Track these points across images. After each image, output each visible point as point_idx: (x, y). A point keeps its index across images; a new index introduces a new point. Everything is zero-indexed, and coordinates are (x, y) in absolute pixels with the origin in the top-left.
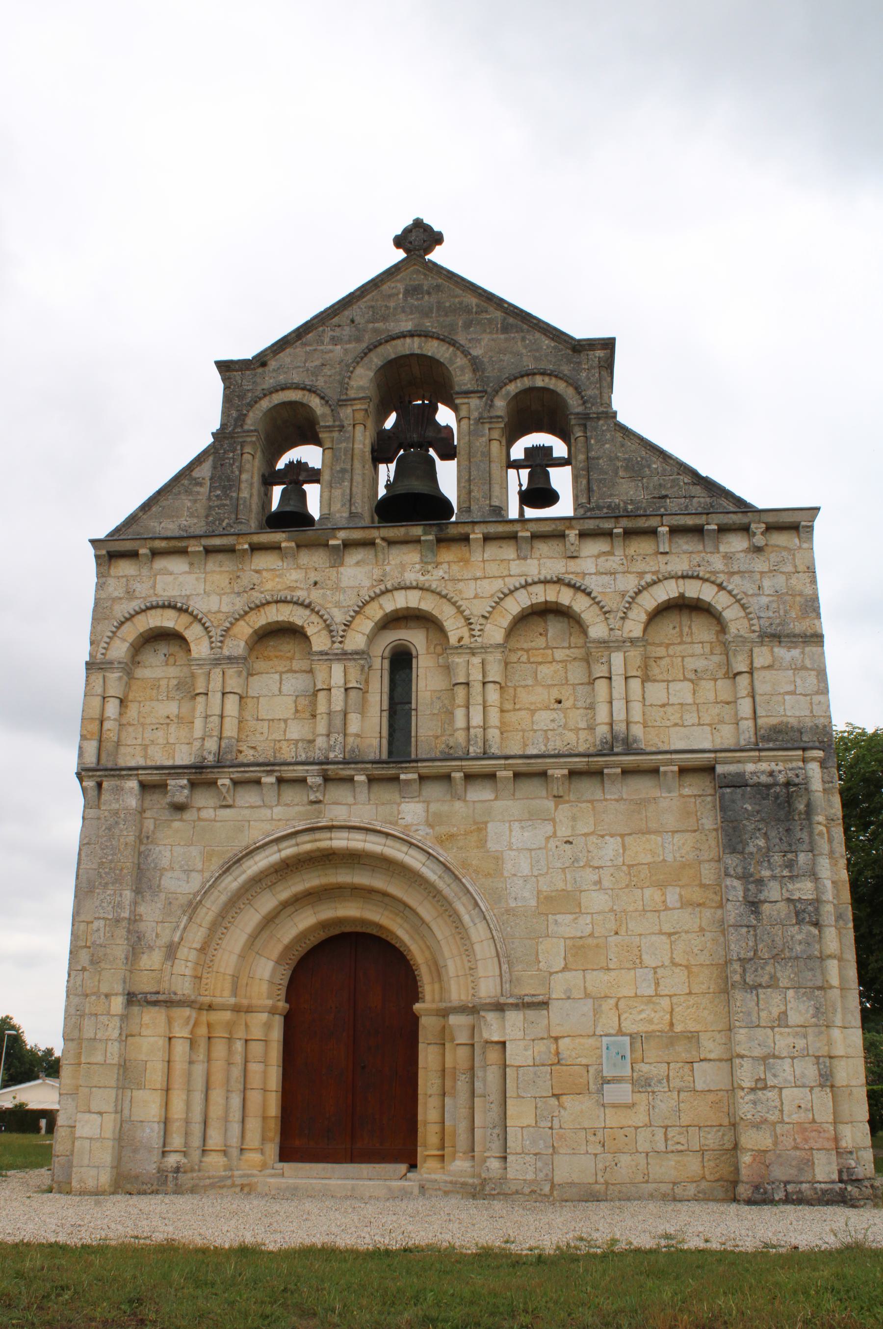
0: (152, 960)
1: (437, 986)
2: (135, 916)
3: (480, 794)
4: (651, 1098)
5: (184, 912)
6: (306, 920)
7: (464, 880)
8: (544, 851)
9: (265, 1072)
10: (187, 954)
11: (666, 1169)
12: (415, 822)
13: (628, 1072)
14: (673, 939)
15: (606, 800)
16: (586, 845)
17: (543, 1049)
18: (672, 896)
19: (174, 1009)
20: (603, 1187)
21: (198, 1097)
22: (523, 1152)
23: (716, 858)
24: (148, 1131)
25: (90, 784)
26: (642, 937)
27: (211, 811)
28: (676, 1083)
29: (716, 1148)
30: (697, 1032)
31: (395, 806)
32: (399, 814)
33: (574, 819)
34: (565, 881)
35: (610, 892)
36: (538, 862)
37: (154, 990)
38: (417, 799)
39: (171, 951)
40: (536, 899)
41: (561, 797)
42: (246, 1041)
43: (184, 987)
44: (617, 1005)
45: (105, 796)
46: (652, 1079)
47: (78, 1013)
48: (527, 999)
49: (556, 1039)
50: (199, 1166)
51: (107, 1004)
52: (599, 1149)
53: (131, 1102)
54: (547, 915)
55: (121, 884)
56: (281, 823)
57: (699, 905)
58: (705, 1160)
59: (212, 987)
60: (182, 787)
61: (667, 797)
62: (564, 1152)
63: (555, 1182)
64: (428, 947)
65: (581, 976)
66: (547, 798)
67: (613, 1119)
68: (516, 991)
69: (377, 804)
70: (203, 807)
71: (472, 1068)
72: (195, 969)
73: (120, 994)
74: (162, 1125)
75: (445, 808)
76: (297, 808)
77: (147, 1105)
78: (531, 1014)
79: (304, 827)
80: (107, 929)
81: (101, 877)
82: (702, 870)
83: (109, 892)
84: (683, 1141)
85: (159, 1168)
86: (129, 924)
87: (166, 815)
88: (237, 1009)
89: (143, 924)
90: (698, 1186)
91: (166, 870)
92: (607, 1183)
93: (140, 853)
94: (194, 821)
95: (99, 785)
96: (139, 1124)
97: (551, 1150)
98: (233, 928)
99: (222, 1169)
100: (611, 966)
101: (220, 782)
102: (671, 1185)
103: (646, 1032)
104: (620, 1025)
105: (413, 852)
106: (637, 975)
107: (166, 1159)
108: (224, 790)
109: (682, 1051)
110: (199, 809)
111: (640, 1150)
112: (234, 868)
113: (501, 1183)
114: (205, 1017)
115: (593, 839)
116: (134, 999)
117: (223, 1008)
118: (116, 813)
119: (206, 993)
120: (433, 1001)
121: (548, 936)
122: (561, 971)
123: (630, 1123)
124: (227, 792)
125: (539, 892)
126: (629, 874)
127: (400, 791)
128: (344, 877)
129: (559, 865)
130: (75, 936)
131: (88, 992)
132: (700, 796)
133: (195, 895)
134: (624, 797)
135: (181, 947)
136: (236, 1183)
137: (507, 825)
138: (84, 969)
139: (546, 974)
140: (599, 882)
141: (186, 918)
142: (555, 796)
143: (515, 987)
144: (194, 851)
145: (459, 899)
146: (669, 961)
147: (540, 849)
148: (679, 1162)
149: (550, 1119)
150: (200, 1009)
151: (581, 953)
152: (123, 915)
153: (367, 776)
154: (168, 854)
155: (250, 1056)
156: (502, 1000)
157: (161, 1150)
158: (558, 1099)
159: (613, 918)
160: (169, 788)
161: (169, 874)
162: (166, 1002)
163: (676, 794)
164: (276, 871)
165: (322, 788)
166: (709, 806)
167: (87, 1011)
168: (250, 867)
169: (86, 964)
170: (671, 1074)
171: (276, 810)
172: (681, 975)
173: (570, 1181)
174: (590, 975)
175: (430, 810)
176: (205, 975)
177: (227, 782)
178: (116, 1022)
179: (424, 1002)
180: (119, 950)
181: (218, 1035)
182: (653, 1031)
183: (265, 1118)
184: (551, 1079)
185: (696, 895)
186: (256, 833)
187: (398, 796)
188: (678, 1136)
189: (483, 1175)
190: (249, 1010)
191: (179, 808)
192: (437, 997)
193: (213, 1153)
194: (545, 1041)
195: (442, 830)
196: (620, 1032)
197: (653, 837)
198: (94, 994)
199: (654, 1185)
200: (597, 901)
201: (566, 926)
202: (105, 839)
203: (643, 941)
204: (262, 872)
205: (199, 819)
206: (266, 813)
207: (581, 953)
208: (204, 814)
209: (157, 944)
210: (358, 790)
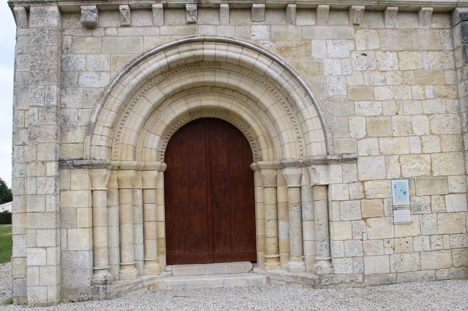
0: (75, 136)
1: (270, 150)
2: (61, 104)
3: (306, 21)
4: (421, 218)
5: (98, 101)
6: (180, 108)
7: (298, 77)
8: (349, 60)
9: (156, 210)
10: (102, 131)
11: (431, 262)
12: (262, 38)
13: (408, 203)
14: (430, 118)
15: (386, 28)
16: (376, 57)
17: (355, 189)
18: (429, 91)
19: (94, 170)
20: (395, 275)
21: (115, 230)
22: (345, 257)
23: (454, 68)
24: (82, 257)
25: (19, 8)
26: (412, 116)
27: (114, 29)
28: (435, 208)
29: (459, 247)
30: (446, 176)
31: (248, 27)
32: (251, 32)
33: (367, 40)
34: (364, 79)
35: (391, 87)
36: (346, 66)
37: (79, 157)
38: (263, 23)
39: (90, 129)
40: (346, 91)
41: (358, 25)
42: (143, 189)
43: (101, 155)
44: (399, 159)
45: (33, 18)
46: (421, 206)
47: (22, 176)
48: (345, 157)
49: (363, 182)
50: (119, 276)
51: (44, 168)
52: (392, 252)
53: (67, 237)
54: (353, 101)
55: (49, 81)
56: (166, 37)
57: (445, 97)
58: (453, 254)
59: (119, 154)
60: (92, 11)
61: (423, 29)
62: (370, 254)
63: (365, 274)
64: (264, 125)
65: (377, 142)
66: (349, 25)
67: (399, 232)
68: (336, 151)
69: (235, 25)
70: (109, 27)
71: (301, 202)
72: (108, 142)
73: (53, 161)
74: (91, 252)
75: (282, 29)
76: (178, 27)
77: (80, 240)
78: (346, 166)
79: (184, 40)
80: (40, 114)
81: (33, 76)
82: (446, 75)
83: (40, 87)
84: (440, 243)
85: (92, 282)
86: (57, 110)
87: (81, 33)
88: (137, 169)
89: (67, 110)
90: (449, 270)
91: (82, 71)
92: (396, 272)
93: (62, 60)
94: (102, 37)
95: (28, 11)
96: (75, 252)
97: (362, 254)
98: (132, 113)
99: (135, 278)
100: (395, 135)
101: (121, 7)
102: (434, 271)
103: (417, 177)
104: (401, 172)
105: (262, 58)
106: (411, 140)
107: (96, 275)
108: (124, 13)
109: (438, 188)
110: (105, 28)
111: (416, 251)
112: (133, 69)
113: (332, 277)
114: (116, 175)
115: (379, 53)
116: (64, 164)
117: (128, 168)
118: (43, 30)
119: (116, 158)
120: (269, 160)
121: (355, 115)
122: (364, 138)
123: (410, 234)
124: (127, 15)
125: (348, 86)
126: (403, 76)
127: (251, 17)
128: (209, 77)
129: (360, 69)
130: (15, 120)
131: (29, 160)
132: (442, 29)
133: (106, 89)
134: (397, 27)
135: (96, 125)
136: (145, 285)
137: (324, 42)
138: (24, 144)
139: (355, 140)
140: (385, 81)
141: (99, 105)
142: (354, 24)
143: (336, 148)
144: (103, 57)
145: (295, 90)
146: (429, 132)
147: (346, 58)
148: (438, 257)
149: (361, 234)
150: (112, 170)
151: (375, 126)
152: (52, 103)
153: (230, 4)
154: (83, 60)
155: (146, 200)
156: (329, 157)
157: (92, 269)
158: (365, 221)
159: (394, 104)
160: (82, 12)
161: (85, 74)
162: (88, 165)
163: (428, 27)
164: (162, 73)
165: (196, 13)
166: (448, 36)
167: (28, 175)
168: (145, 69)
169: (26, 140)
170: (432, 203)
171: (162, 28)
172: (436, 140)
173: (374, 273)
174: (382, 141)
175: (272, 30)
176: (114, 146)
177: (127, 7)
178: (52, 181)
179: (261, 160)
180: (51, 129)
181: (125, 187)
182: (421, 176)
183: (158, 239)
184: (361, 209)
185: (443, 91)
186: (150, 44)
187: (250, 20)
188: (437, 241)
189: (318, 273)
190: (144, 169)
191: (90, 27)
192: (271, 157)
193: (127, 267)
194: (356, 184)
195: (281, 44)
196: (402, 177)
197: (415, 53)
198: (33, 161)
199: (424, 272)
200: (384, 93)
201: (365, 108)
202: (34, 48)
203: (413, 119)
204: (153, 72)
205: (106, 35)
206: (156, 30)
207: (375, 126)
208: (109, 32)
209: (79, 124)
210: (222, 15)
